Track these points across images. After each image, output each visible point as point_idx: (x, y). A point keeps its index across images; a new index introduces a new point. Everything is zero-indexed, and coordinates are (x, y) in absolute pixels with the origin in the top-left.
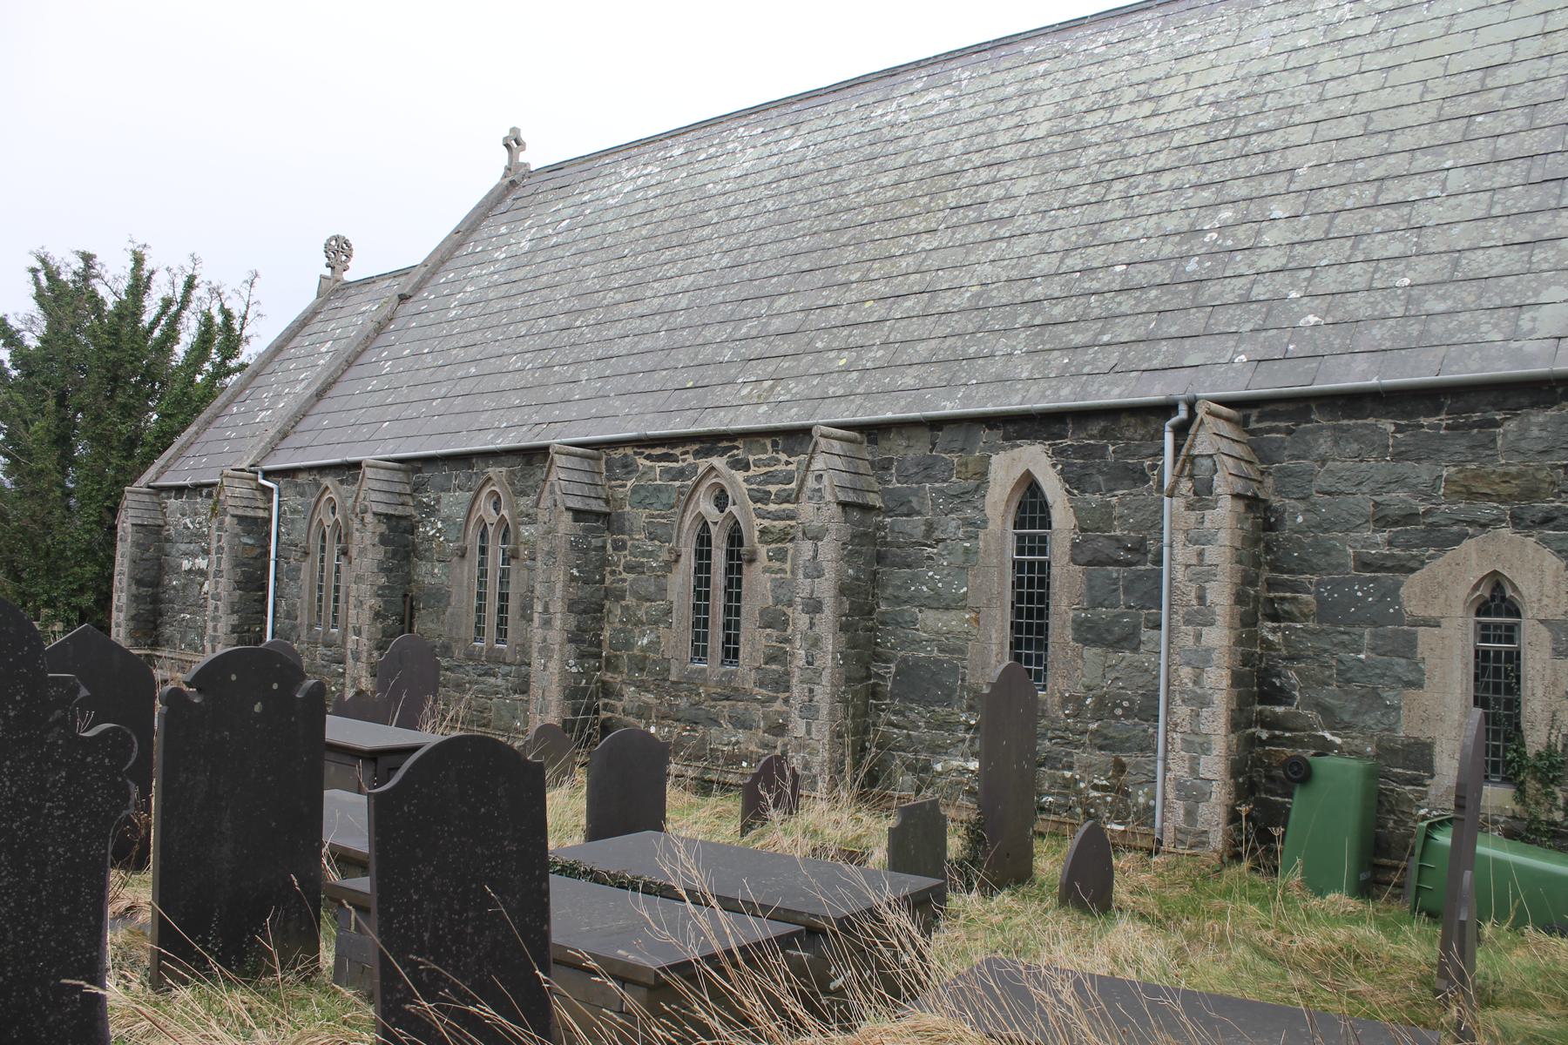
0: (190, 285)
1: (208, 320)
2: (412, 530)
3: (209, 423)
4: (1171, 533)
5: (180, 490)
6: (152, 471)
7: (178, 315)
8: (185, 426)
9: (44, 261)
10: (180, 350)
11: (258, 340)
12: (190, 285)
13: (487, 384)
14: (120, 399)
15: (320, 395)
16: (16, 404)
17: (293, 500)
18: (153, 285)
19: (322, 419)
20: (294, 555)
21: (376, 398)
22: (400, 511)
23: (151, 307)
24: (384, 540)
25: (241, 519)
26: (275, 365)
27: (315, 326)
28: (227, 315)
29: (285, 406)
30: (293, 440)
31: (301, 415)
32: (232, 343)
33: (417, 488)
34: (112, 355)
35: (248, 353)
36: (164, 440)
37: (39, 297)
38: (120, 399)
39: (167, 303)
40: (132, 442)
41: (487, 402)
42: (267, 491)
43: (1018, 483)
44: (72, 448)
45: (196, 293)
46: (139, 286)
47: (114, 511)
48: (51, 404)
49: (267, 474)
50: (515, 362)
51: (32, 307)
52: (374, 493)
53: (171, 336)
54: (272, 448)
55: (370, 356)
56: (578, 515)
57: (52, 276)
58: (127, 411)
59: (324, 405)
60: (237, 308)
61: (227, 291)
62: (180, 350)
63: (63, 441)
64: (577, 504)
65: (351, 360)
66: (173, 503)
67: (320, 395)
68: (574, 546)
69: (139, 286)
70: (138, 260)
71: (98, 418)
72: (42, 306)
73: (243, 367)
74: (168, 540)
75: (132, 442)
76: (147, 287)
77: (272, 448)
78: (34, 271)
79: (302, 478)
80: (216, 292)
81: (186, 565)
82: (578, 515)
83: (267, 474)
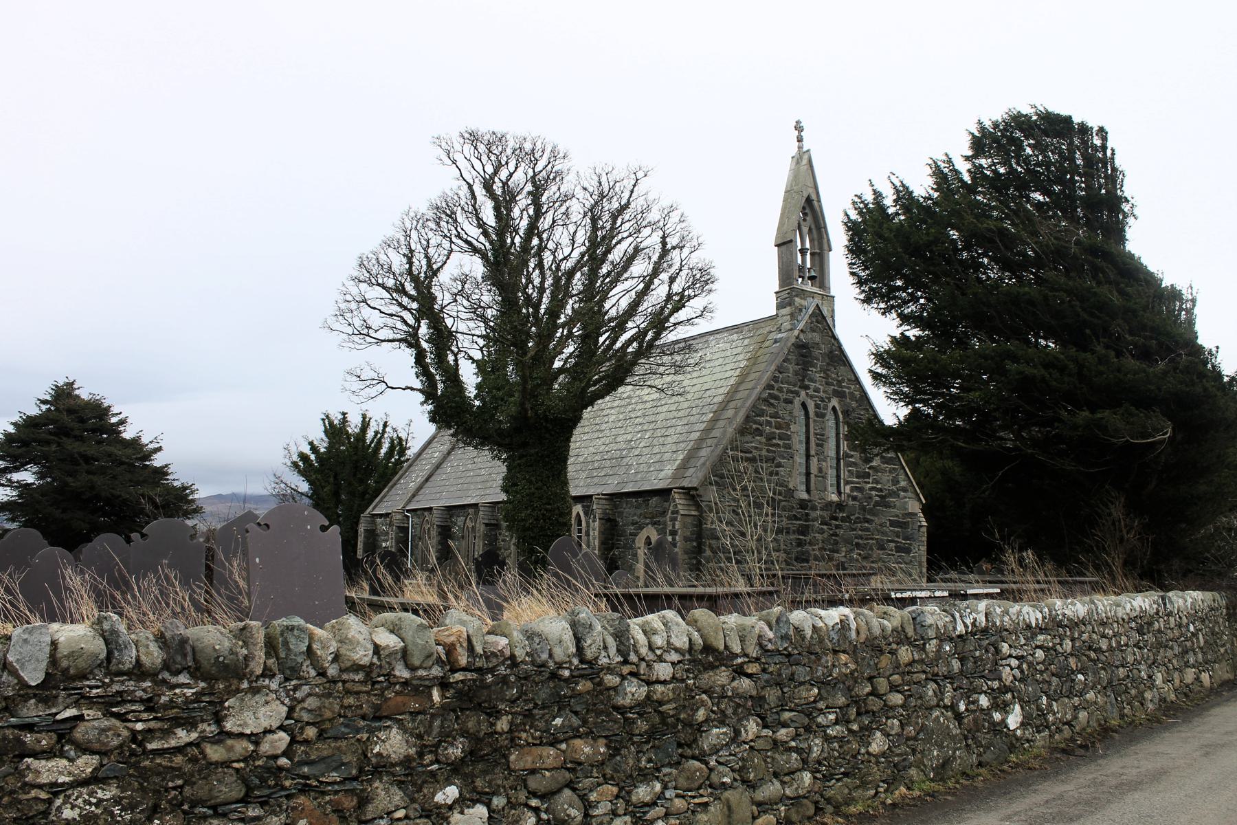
0: (385, 425)
1: (392, 441)
2: (450, 530)
3: (392, 487)
4: (1090, 582)
5: (381, 515)
6: (371, 508)
7: (381, 438)
8: (385, 486)
9: (327, 417)
10: (383, 451)
11: (414, 447)
12: (385, 425)
13: (475, 479)
14: (359, 476)
15: (427, 480)
16: (319, 480)
17: (416, 520)
18: (371, 424)
19: (426, 491)
20: (417, 539)
21: (443, 483)
22: (445, 524)
23: (370, 434)
24: (440, 534)
25: (398, 527)
26: (418, 462)
27: (434, 444)
28: (400, 439)
29: (413, 485)
30: (417, 498)
31: (420, 488)
32: (403, 451)
33: (451, 516)
34: (355, 458)
35: (410, 453)
36: (377, 492)
37: (326, 432)
38: (359, 476)
39: (376, 433)
40: (364, 493)
41: (472, 487)
42: (408, 517)
43: (233, 497)
44: (340, 496)
45: (388, 429)
46: (365, 425)
47: (357, 523)
48: (332, 479)
49: (408, 511)
50: (483, 472)
51: (323, 435)
52: (436, 519)
53: (379, 445)
54: (409, 501)
55: (444, 465)
56: (487, 525)
57: (331, 423)
58: (361, 481)
59: (428, 484)
60: (403, 435)
61: (400, 430)
62: (383, 451)
63: (336, 494)
64: (486, 522)
65: (438, 466)
66: (379, 520)
67: (427, 480)
68: (486, 535)
69: (365, 425)
70: (364, 417)
71: (350, 484)
72: (327, 436)
73: (408, 460)
74: (377, 535)
75: (364, 493)
76: (368, 424)
77: (409, 501)
78: (323, 420)
79: (419, 512)
80: (395, 430)
81: (384, 545)
82: (487, 525)
83: (408, 511)
